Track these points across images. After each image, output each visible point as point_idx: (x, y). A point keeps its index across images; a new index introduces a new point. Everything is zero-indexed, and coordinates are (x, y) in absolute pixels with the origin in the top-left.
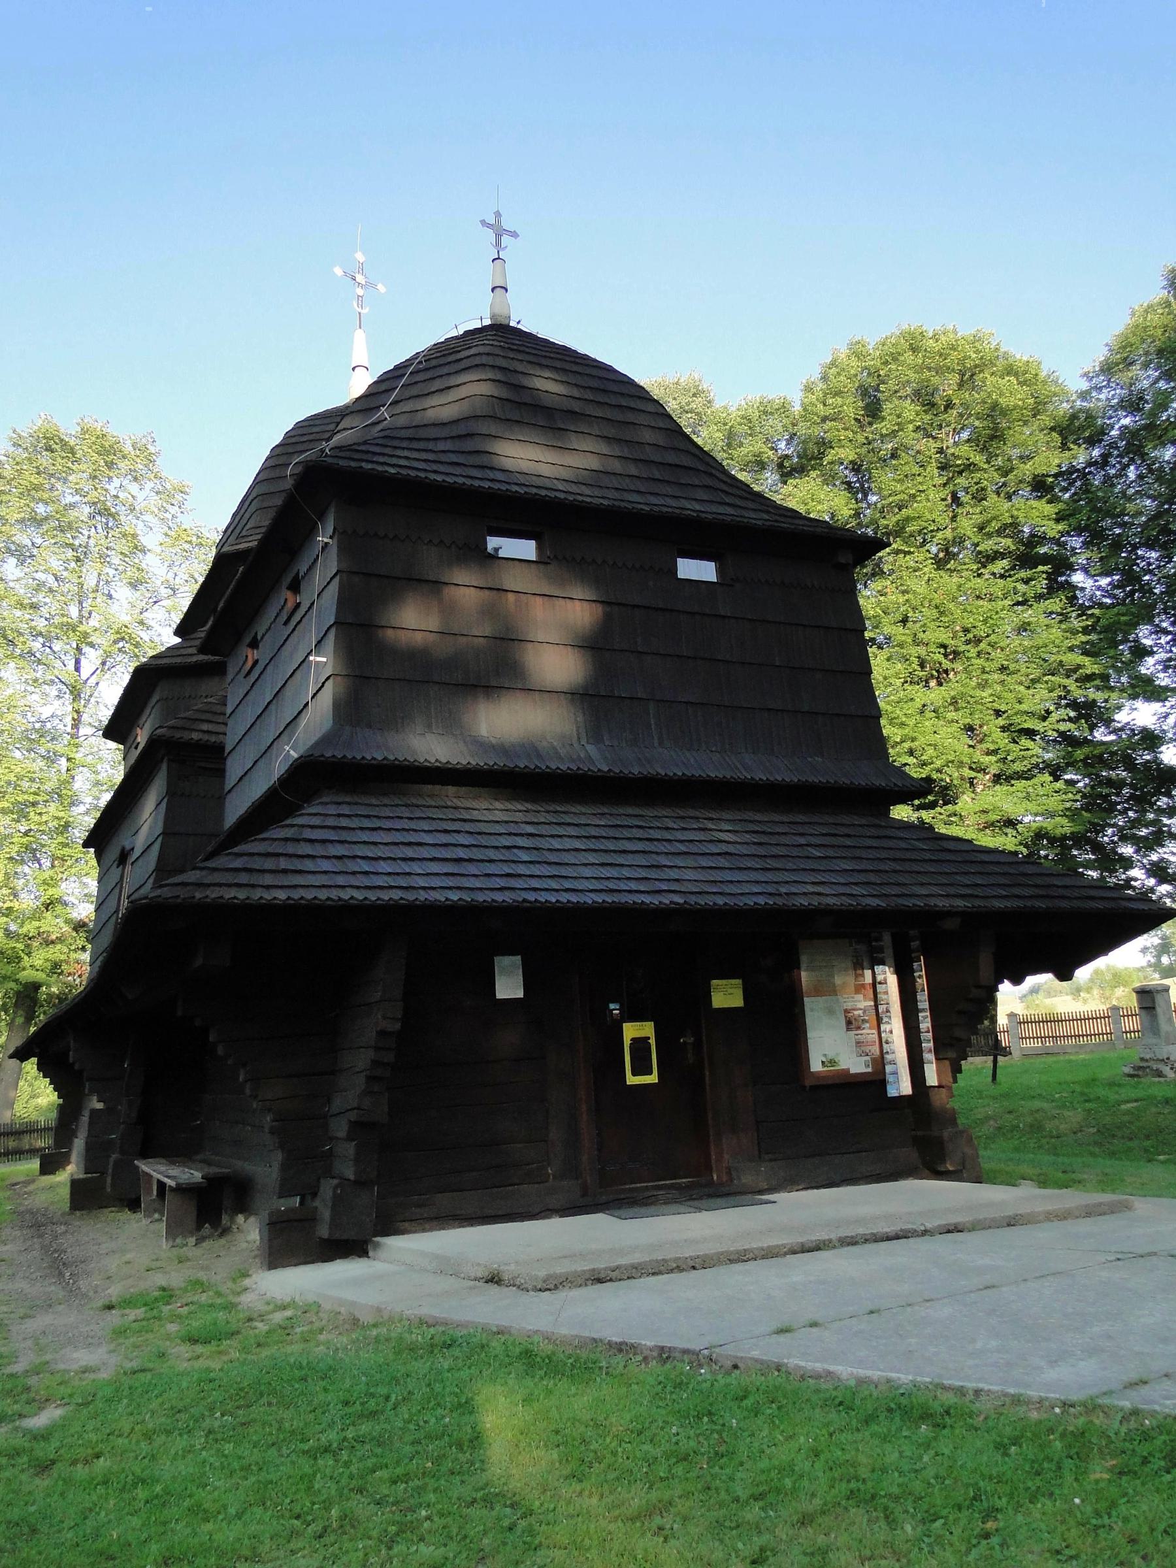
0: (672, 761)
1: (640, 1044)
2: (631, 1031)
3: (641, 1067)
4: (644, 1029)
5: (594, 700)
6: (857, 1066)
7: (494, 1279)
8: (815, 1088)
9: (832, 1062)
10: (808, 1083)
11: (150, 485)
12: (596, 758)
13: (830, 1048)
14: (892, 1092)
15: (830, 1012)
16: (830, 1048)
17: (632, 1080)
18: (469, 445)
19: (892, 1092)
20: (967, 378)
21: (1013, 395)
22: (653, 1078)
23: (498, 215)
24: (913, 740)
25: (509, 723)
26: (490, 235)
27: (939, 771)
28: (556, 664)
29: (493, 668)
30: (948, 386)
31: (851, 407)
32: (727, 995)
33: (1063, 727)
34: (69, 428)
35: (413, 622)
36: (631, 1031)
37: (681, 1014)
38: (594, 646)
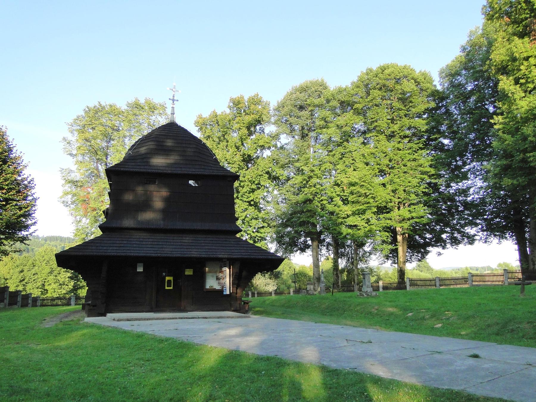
0: (179, 225)
1: (169, 281)
2: (167, 278)
3: (169, 285)
4: (171, 278)
5: (165, 212)
6: (218, 287)
7: (114, 320)
8: (206, 292)
9: (212, 287)
10: (205, 290)
11: (164, 117)
12: (162, 224)
13: (211, 283)
14: (225, 293)
15: (213, 276)
16: (211, 283)
17: (166, 288)
18: (145, 160)
19: (225, 293)
20: (398, 81)
21: (408, 86)
22: (171, 288)
23: (174, 96)
24: (373, 194)
25: (148, 216)
26: (171, 101)
27: (380, 204)
28: (158, 204)
29: (145, 205)
30: (391, 84)
31: (362, 92)
32: (189, 272)
33: (424, 190)
34: (142, 101)
35: (129, 197)
36: (167, 278)
37: (178, 276)
38: (167, 200)
